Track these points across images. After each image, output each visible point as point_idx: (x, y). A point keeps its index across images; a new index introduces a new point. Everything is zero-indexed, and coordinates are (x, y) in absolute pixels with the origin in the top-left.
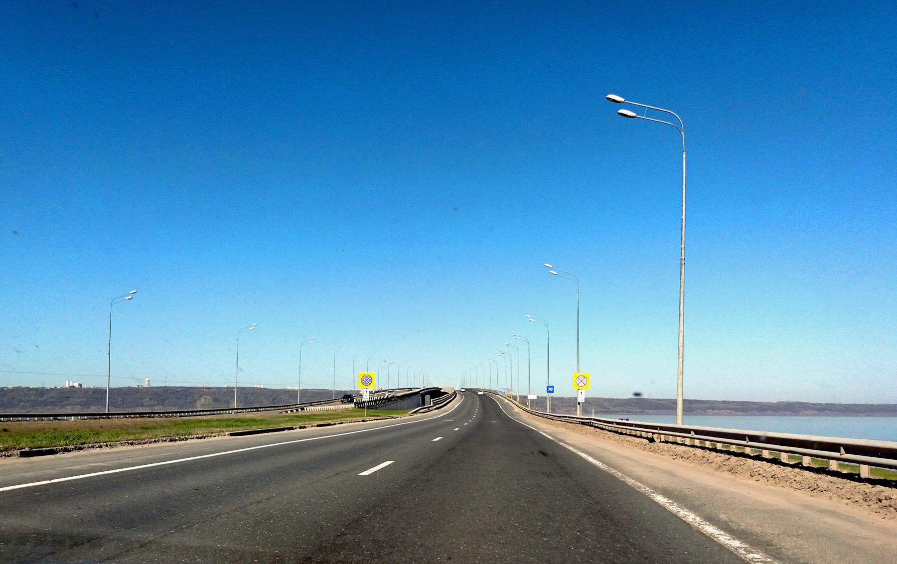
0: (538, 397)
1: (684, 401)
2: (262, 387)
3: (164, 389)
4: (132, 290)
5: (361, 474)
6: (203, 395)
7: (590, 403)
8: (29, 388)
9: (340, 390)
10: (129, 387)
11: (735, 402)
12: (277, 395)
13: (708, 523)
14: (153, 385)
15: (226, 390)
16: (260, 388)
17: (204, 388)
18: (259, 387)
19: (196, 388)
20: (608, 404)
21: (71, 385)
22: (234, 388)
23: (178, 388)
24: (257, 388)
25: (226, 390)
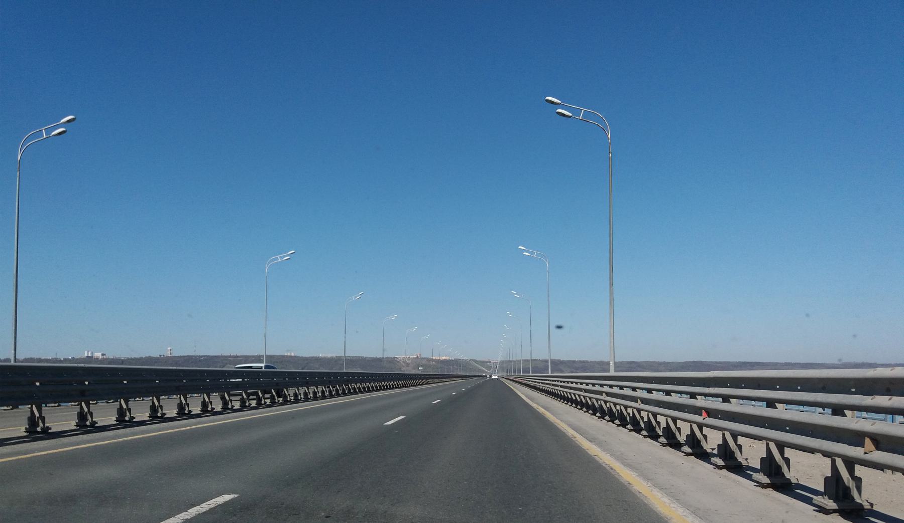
0: (18, 408)
1: (615, 363)
2: (293, 355)
3: (185, 358)
4: (291, 251)
5: (404, 417)
6: (226, 364)
7: (619, 366)
8: (40, 359)
9: (375, 357)
10: (149, 356)
11: (798, 363)
12: (307, 363)
13: (604, 465)
14: (175, 354)
15: (253, 359)
16: (291, 356)
17: (230, 356)
18: (289, 355)
19: (222, 356)
20: (664, 368)
21: (90, 355)
22: (263, 356)
23: (202, 356)
24: (287, 356)
25: (253, 359)
